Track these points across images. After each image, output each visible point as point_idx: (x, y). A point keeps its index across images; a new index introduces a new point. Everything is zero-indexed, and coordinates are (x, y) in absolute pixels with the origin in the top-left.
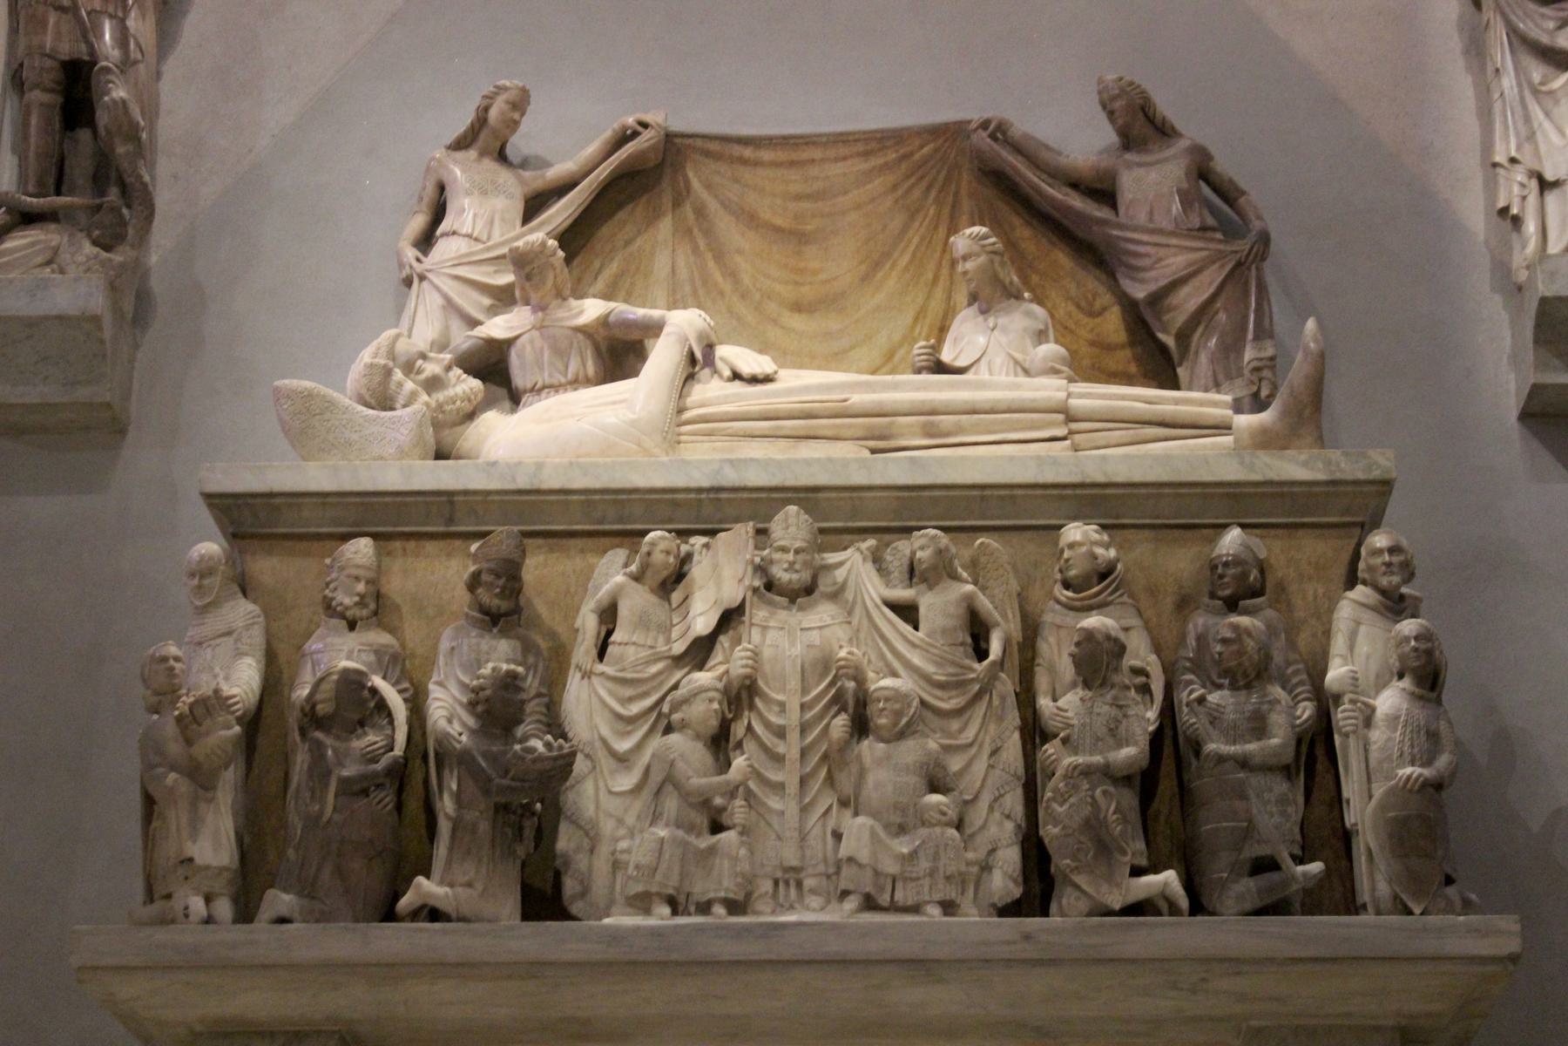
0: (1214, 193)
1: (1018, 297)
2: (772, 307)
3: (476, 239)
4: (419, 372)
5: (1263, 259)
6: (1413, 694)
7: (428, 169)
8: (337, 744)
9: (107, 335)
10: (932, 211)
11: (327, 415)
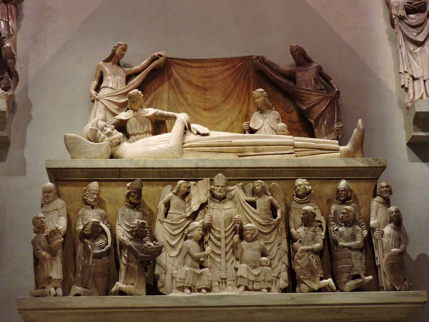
0: (322, 76)
1: (271, 109)
2: (197, 109)
3: (113, 89)
4: (105, 131)
5: (338, 98)
6: (394, 228)
7: (98, 68)
8: (92, 243)
9: (7, 117)
10: (242, 82)
11: (80, 144)
